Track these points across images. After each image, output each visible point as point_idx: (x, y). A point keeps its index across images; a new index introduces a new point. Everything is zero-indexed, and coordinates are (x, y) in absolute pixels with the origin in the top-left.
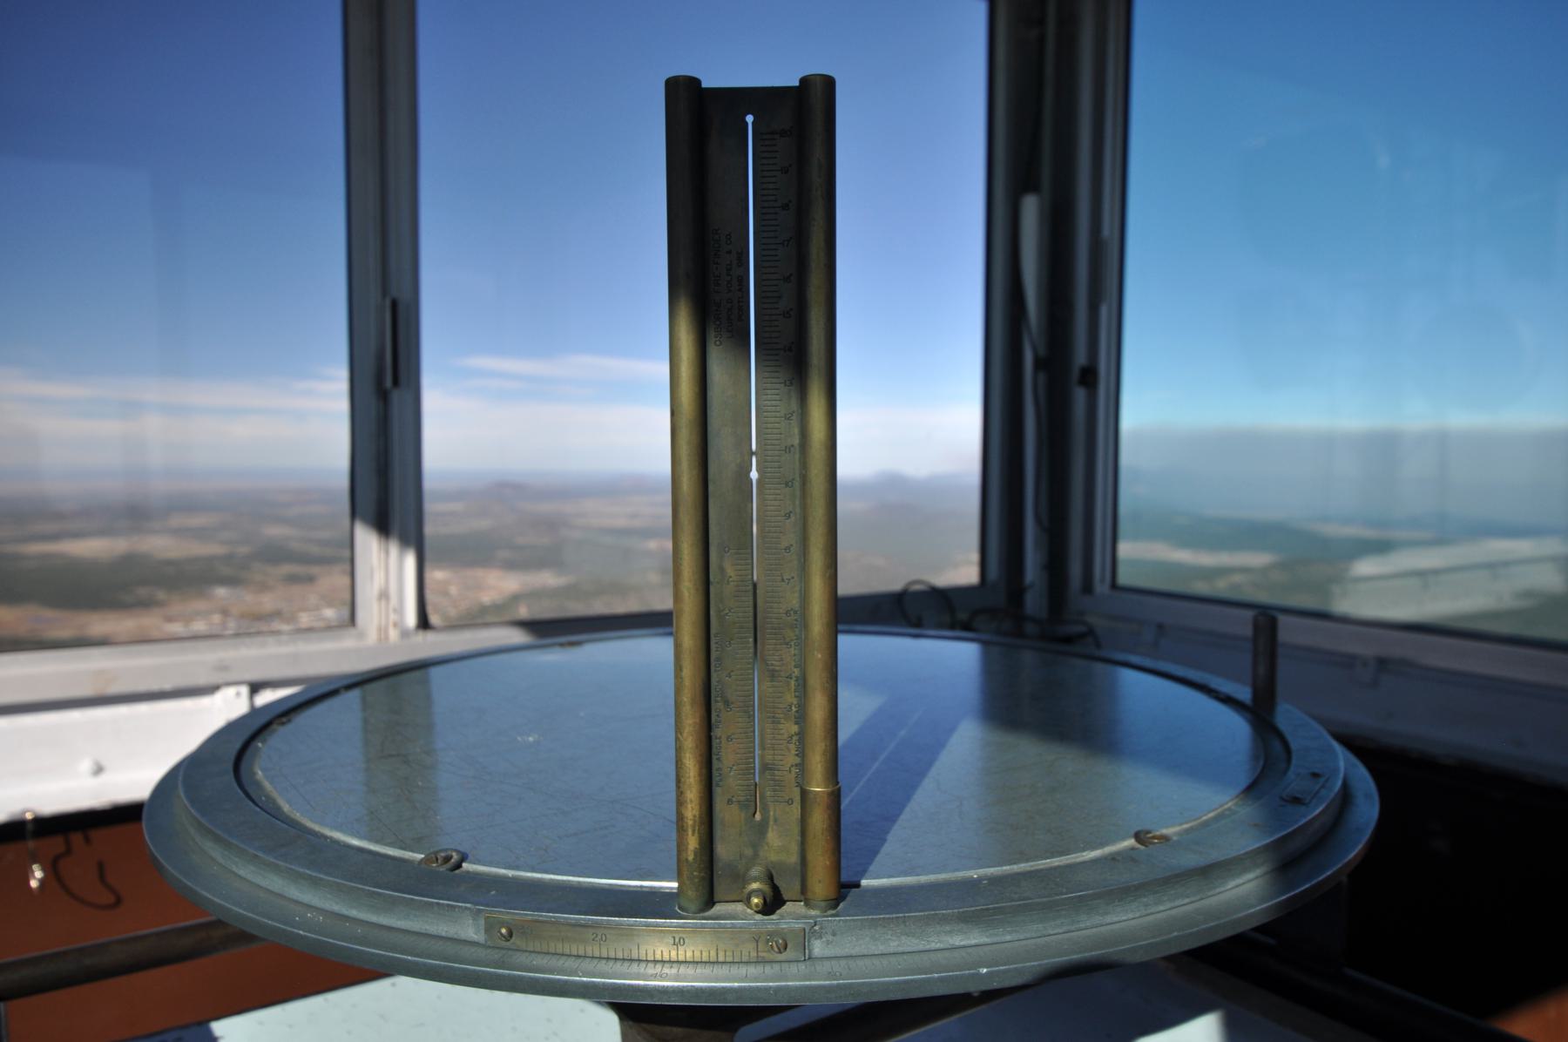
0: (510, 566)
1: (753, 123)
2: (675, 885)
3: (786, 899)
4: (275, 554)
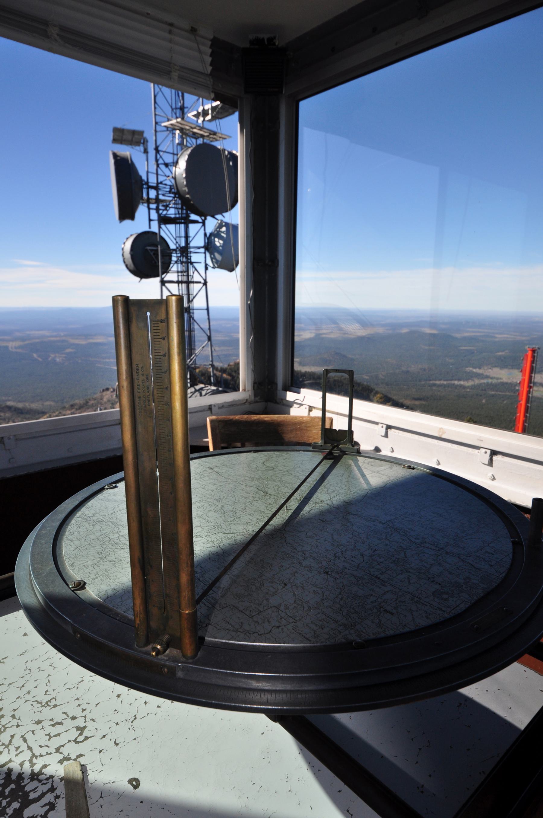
1: (150, 316)
3: (20, 725)
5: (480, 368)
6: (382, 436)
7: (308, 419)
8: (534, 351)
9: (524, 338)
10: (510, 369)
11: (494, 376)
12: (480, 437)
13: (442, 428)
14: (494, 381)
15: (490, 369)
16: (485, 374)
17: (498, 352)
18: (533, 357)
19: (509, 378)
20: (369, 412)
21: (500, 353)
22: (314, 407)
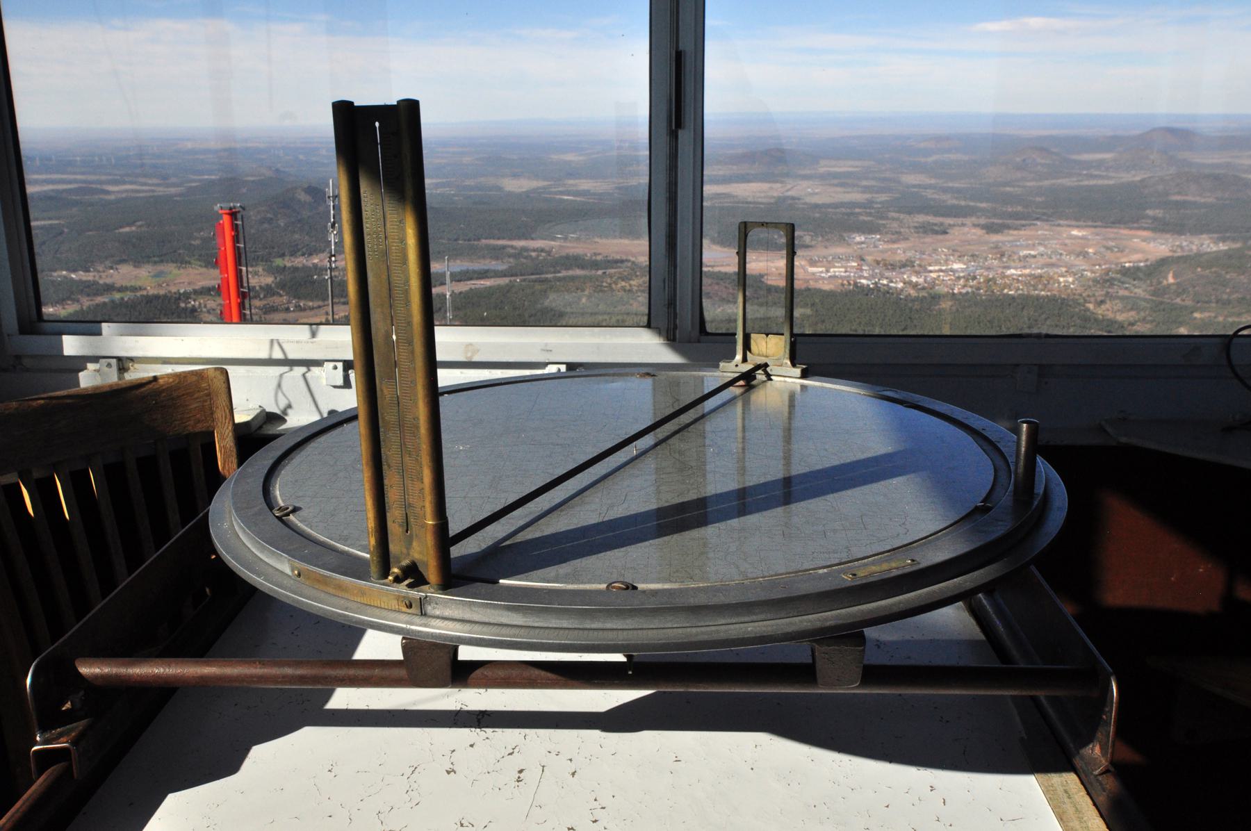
0: (1162, 227)
1: (379, 127)
2: (980, 595)
4: (912, 203)
5: (87, 270)
6: (335, 387)
7: (171, 380)
8: (233, 214)
9: (173, 190)
10: (155, 263)
11: (125, 283)
12: (546, 345)
13: (471, 344)
14: (127, 296)
15: (111, 268)
16: (101, 282)
17: (121, 227)
18: (235, 228)
19: (160, 285)
20: (297, 342)
21: (127, 229)
22: (131, 359)
